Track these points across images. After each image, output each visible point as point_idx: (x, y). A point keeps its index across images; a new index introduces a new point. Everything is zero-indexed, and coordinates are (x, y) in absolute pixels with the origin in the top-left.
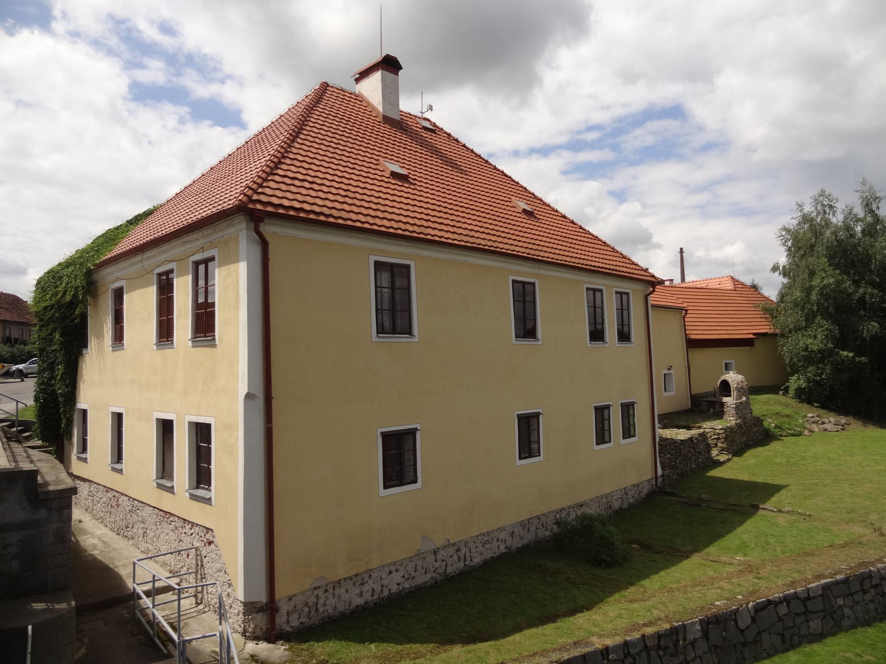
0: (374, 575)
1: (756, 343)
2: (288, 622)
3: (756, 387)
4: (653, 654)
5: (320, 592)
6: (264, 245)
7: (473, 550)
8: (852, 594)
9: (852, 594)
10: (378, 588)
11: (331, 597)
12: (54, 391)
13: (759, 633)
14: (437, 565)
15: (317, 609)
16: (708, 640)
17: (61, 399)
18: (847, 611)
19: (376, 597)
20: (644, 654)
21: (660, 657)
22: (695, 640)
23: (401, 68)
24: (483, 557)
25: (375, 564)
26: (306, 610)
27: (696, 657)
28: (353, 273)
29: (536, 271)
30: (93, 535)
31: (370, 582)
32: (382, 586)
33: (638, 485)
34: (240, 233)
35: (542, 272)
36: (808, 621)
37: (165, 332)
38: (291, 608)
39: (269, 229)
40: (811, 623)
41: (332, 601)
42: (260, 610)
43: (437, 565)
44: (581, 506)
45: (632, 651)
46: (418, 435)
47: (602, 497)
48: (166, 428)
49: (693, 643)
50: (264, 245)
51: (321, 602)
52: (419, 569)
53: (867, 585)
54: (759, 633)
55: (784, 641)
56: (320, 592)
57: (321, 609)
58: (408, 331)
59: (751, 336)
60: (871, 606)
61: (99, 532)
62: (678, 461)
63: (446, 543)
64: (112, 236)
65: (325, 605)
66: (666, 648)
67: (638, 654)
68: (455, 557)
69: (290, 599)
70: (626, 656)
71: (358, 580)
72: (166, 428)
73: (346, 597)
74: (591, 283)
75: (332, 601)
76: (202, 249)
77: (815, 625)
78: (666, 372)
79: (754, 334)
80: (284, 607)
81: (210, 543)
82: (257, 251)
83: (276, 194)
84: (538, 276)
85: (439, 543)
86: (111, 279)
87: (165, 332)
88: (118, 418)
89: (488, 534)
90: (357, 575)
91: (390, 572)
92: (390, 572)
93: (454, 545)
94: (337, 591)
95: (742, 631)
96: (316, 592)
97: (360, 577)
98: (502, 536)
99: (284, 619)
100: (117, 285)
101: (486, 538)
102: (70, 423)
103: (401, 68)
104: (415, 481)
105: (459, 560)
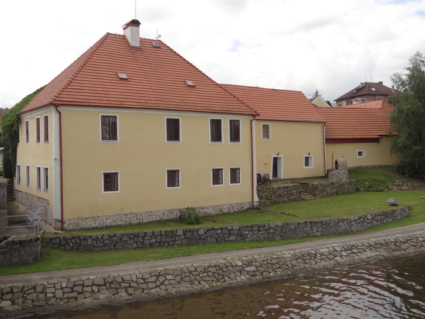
0: (100, 218)
1: (381, 141)
2: (68, 227)
3: (381, 166)
4: (163, 236)
5: (80, 220)
6: (60, 113)
7: (144, 217)
8: (253, 231)
9: (253, 231)
10: (102, 223)
11: (83, 222)
12: (9, 159)
13: (207, 237)
14: (127, 219)
15: (78, 225)
16: (185, 236)
17: (11, 162)
18: (249, 236)
19: (101, 225)
20: (160, 236)
21: (165, 238)
22: (180, 235)
23: (140, 24)
24: (148, 220)
25: (100, 215)
26: (75, 224)
27: (179, 240)
28: (94, 119)
29: (179, 114)
30: (21, 209)
31: (99, 220)
32: (103, 222)
33: (241, 204)
34: (53, 109)
35: (181, 114)
36: (230, 236)
37: (38, 140)
38: (69, 223)
39: (60, 109)
40: (231, 237)
41: (84, 224)
42: (59, 222)
43: (127, 219)
44: (203, 208)
45: (155, 234)
46: (119, 175)
47: (216, 206)
48: (39, 169)
49: (179, 236)
50: (60, 113)
51: (80, 223)
52: (119, 220)
53: (261, 229)
54: (207, 237)
55: (217, 241)
56: (80, 220)
57: (80, 226)
58: (116, 139)
59: (378, 137)
60: (262, 236)
61: (23, 208)
62: (273, 196)
63: (131, 213)
64: (27, 100)
65: (81, 224)
66: (168, 236)
67: (157, 235)
68: (135, 218)
69: (69, 220)
70: (153, 235)
71: (93, 218)
72: (39, 169)
73: (89, 223)
74: (212, 117)
75: (84, 224)
76: (45, 113)
77: (232, 238)
78: (307, 156)
79: (379, 135)
80: (67, 222)
81: (48, 204)
82: (58, 115)
83: (65, 98)
84: (180, 116)
85: (127, 212)
86: (26, 118)
87: (38, 140)
88: (28, 167)
89: (151, 212)
90: (93, 217)
91: (107, 219)
92: (107, 219)
93: (134, 214)
94: (86, 221)
95: (200, 235)
96: (78, 220)
97: (94, 218)
98: (158, 214)
99: (67, 226)
100: (27, 120)
101: (150, 213)
102: (15, 170)
103: (140, 24)
104: (117, 190)
105: (137, 219)
